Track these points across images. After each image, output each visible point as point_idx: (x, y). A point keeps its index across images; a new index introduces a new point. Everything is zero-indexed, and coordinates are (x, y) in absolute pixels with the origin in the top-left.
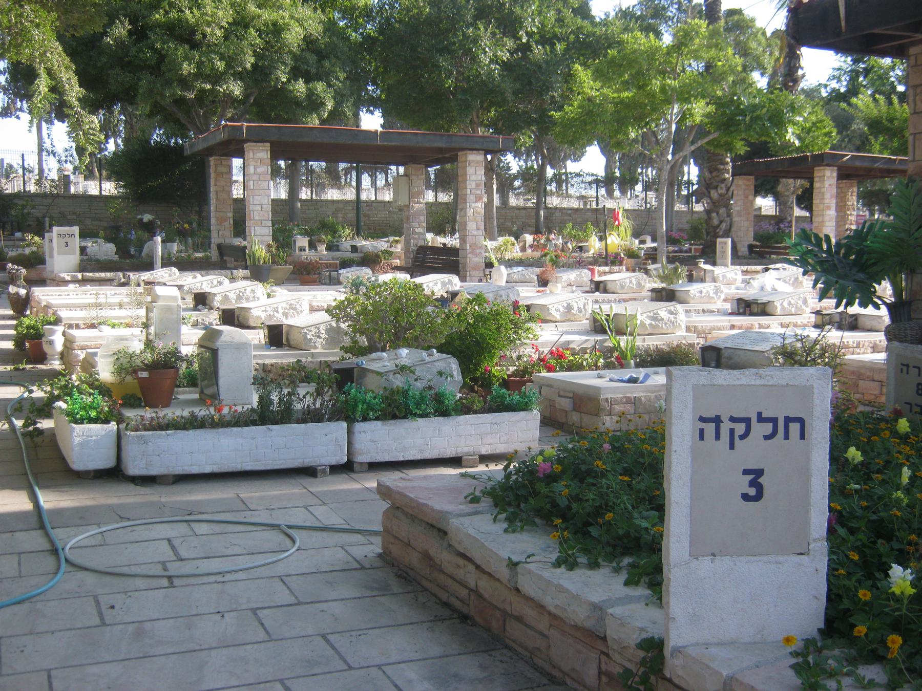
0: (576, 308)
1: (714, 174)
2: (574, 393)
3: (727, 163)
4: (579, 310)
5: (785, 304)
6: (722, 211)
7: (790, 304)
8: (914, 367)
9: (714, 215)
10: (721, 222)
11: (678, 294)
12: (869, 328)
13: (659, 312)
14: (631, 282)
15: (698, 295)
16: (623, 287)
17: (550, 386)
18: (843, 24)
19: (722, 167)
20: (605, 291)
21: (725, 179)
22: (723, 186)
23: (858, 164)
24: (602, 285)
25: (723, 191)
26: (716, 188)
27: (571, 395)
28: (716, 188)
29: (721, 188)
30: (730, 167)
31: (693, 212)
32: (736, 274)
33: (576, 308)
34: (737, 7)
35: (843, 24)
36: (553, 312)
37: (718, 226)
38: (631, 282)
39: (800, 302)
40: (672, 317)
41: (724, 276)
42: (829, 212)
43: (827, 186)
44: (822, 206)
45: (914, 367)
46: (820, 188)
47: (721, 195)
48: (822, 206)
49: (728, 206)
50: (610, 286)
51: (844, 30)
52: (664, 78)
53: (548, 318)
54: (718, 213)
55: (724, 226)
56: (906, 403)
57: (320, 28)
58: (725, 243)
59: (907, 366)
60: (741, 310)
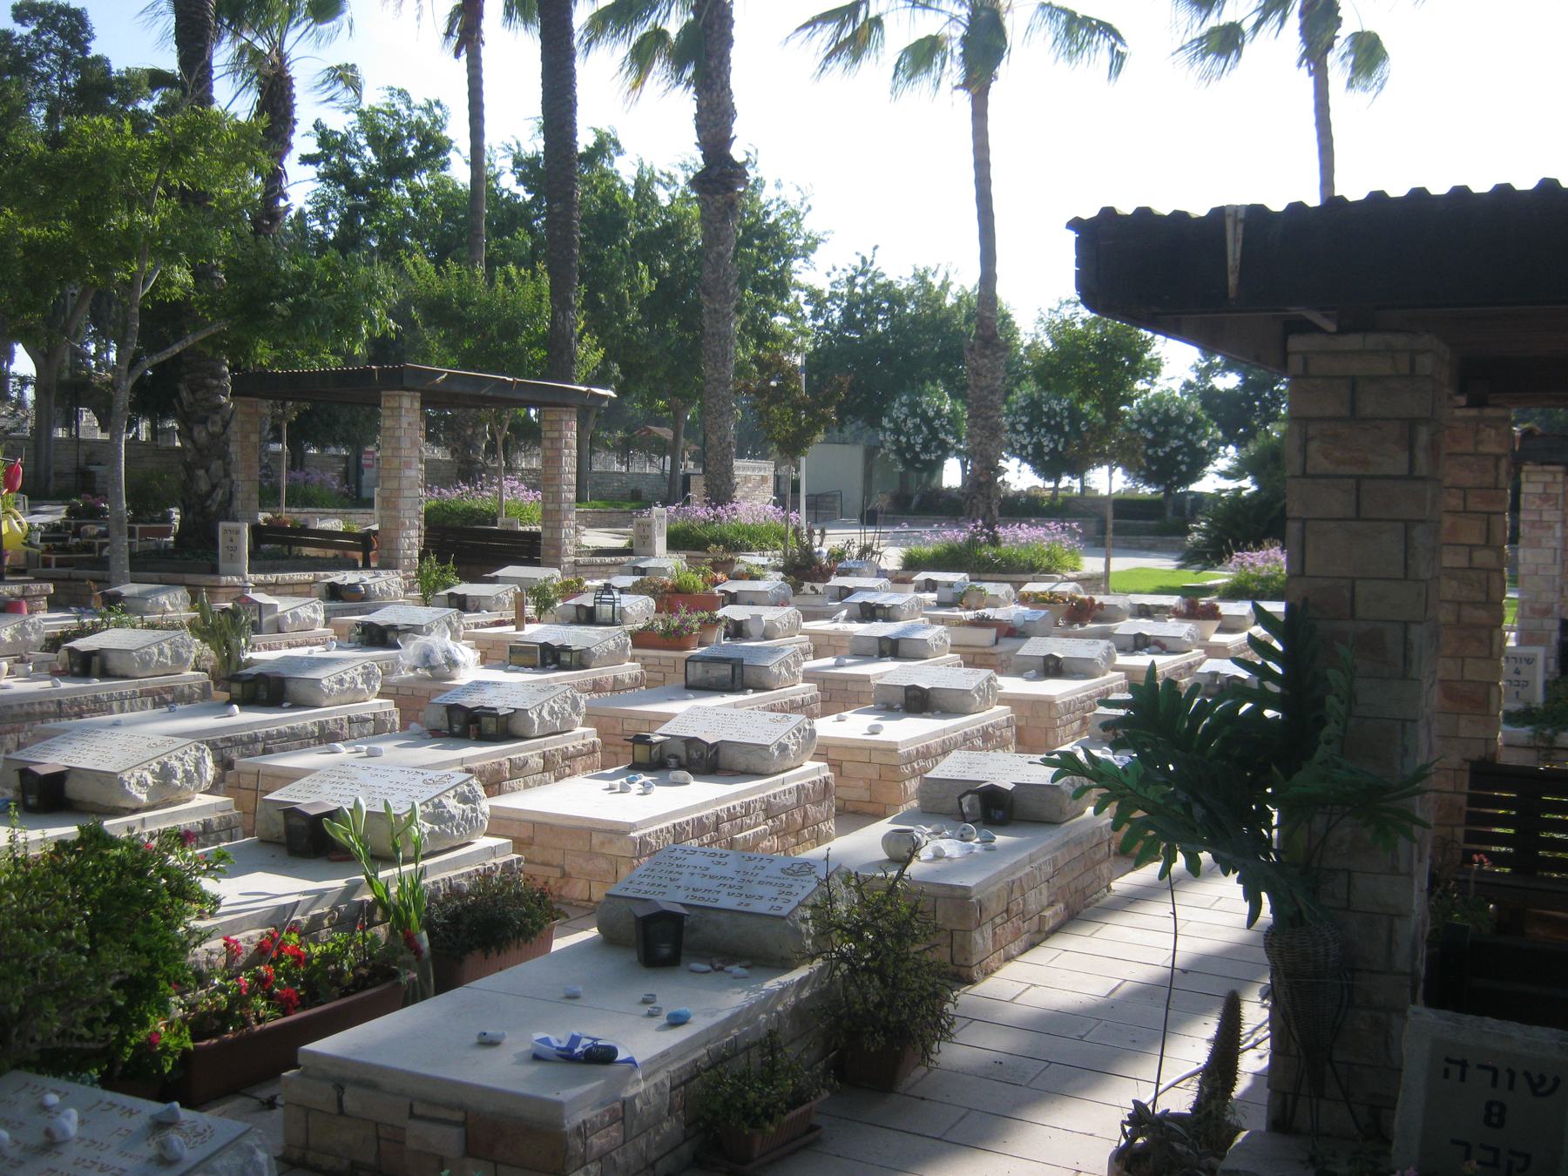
0: (180, 775)
1: (200, 395)
2: (461, 1107)
3: (224, 375)
4: (188, 776)
5: (545, 714)
6: (216, 465)
7: (552, 712)
8: (1481, 1067)
9: (201, 472)
10: (214, 487)
11: (291, 686)
12: (742, 767)
13: (445, 801)
14: (161, 652)
15: (336, 687)
16: (145, 664)
17: (372, 1085)
18: (1232, 280)
19: (215, 382)
20: (105, 674)
21: (221, 406)
22: (217, 418)
23: (456, 388)
24: (96, 660)
25: (217, 429)
26: (204, 421)
27: (459, 1116)
28: (204, 421)
29: (214, 423)
30: (227, 383)
31: (79, 442)
32: (315, 611)
33: (180, 775)
34: (623, 145)
35: (1232, 280)
36: (134, 790)
37: (209, 495)
38: (161, 652)
39: (568, 707)
40: (467, 807)
41: (295, 616)
42: (408, 473)
43: (405, 425)
44: (396, 461)
45: (1481, 1067)
46: (394, 428)
47: (212, 436)
48: (396, 461)
49: (224, 456)
50: (114, 663)
51: (1232, 295)
52: (131, 211)
53: (123, 804)
54: (207, 471)
55: (219, 494)
56: (1454, 1142)
57: (1028, 342)
58: (238, 532)
59: (1464, 1064)
60: (457, 728)
